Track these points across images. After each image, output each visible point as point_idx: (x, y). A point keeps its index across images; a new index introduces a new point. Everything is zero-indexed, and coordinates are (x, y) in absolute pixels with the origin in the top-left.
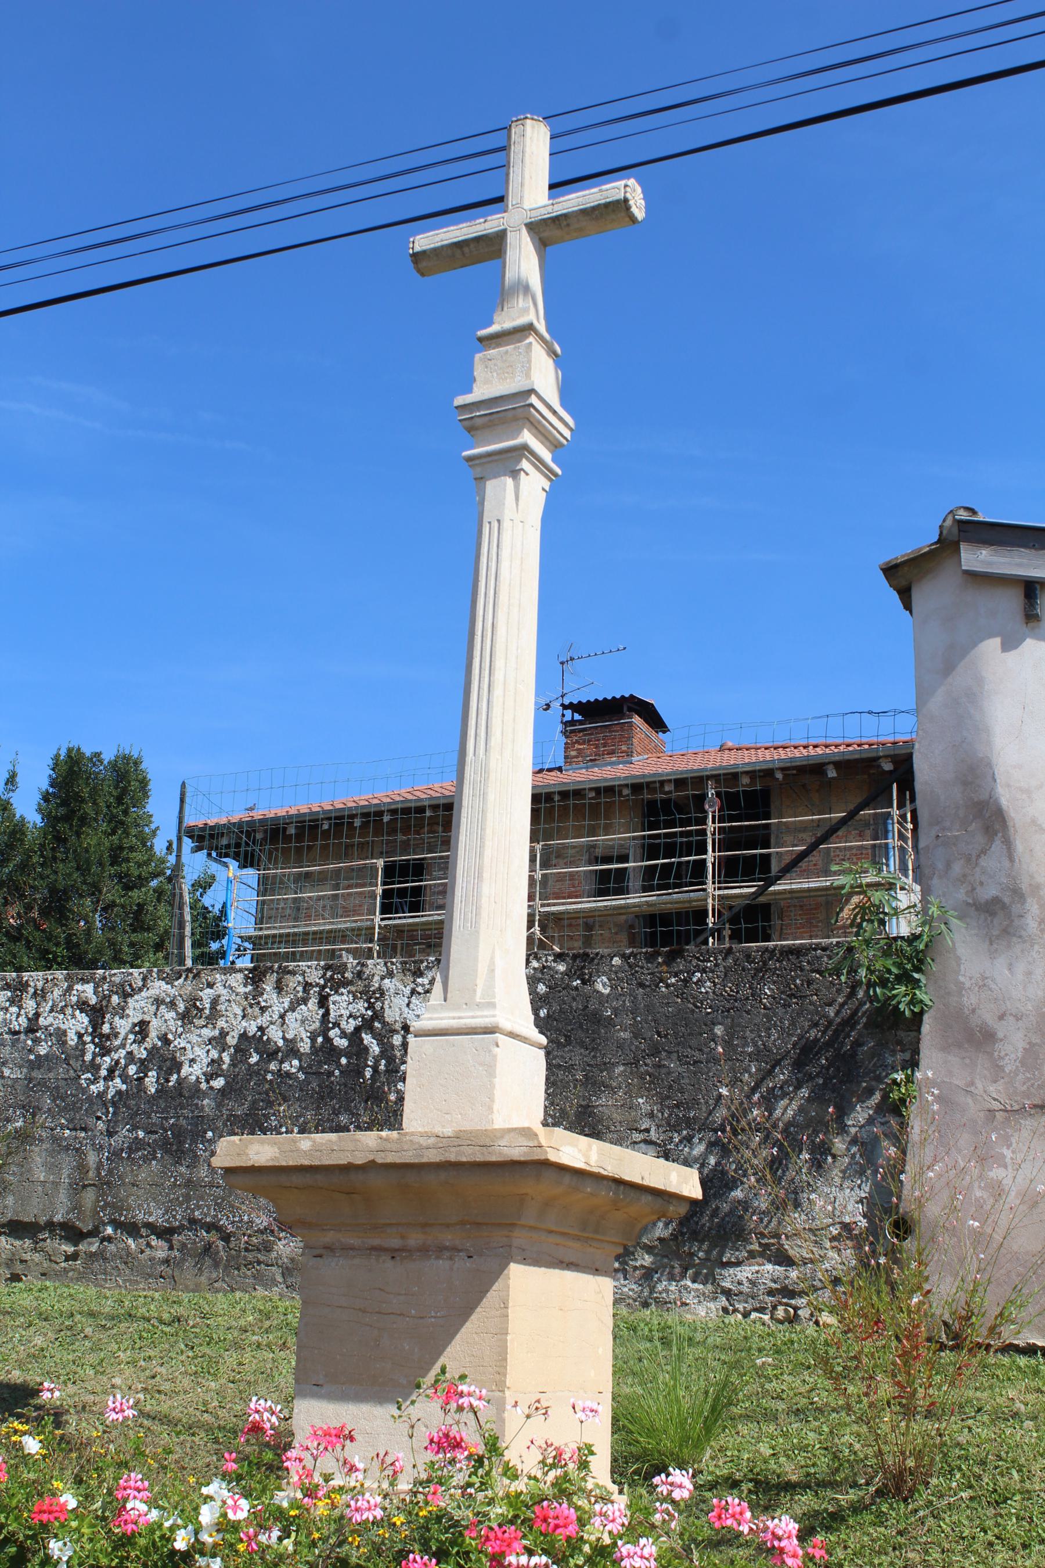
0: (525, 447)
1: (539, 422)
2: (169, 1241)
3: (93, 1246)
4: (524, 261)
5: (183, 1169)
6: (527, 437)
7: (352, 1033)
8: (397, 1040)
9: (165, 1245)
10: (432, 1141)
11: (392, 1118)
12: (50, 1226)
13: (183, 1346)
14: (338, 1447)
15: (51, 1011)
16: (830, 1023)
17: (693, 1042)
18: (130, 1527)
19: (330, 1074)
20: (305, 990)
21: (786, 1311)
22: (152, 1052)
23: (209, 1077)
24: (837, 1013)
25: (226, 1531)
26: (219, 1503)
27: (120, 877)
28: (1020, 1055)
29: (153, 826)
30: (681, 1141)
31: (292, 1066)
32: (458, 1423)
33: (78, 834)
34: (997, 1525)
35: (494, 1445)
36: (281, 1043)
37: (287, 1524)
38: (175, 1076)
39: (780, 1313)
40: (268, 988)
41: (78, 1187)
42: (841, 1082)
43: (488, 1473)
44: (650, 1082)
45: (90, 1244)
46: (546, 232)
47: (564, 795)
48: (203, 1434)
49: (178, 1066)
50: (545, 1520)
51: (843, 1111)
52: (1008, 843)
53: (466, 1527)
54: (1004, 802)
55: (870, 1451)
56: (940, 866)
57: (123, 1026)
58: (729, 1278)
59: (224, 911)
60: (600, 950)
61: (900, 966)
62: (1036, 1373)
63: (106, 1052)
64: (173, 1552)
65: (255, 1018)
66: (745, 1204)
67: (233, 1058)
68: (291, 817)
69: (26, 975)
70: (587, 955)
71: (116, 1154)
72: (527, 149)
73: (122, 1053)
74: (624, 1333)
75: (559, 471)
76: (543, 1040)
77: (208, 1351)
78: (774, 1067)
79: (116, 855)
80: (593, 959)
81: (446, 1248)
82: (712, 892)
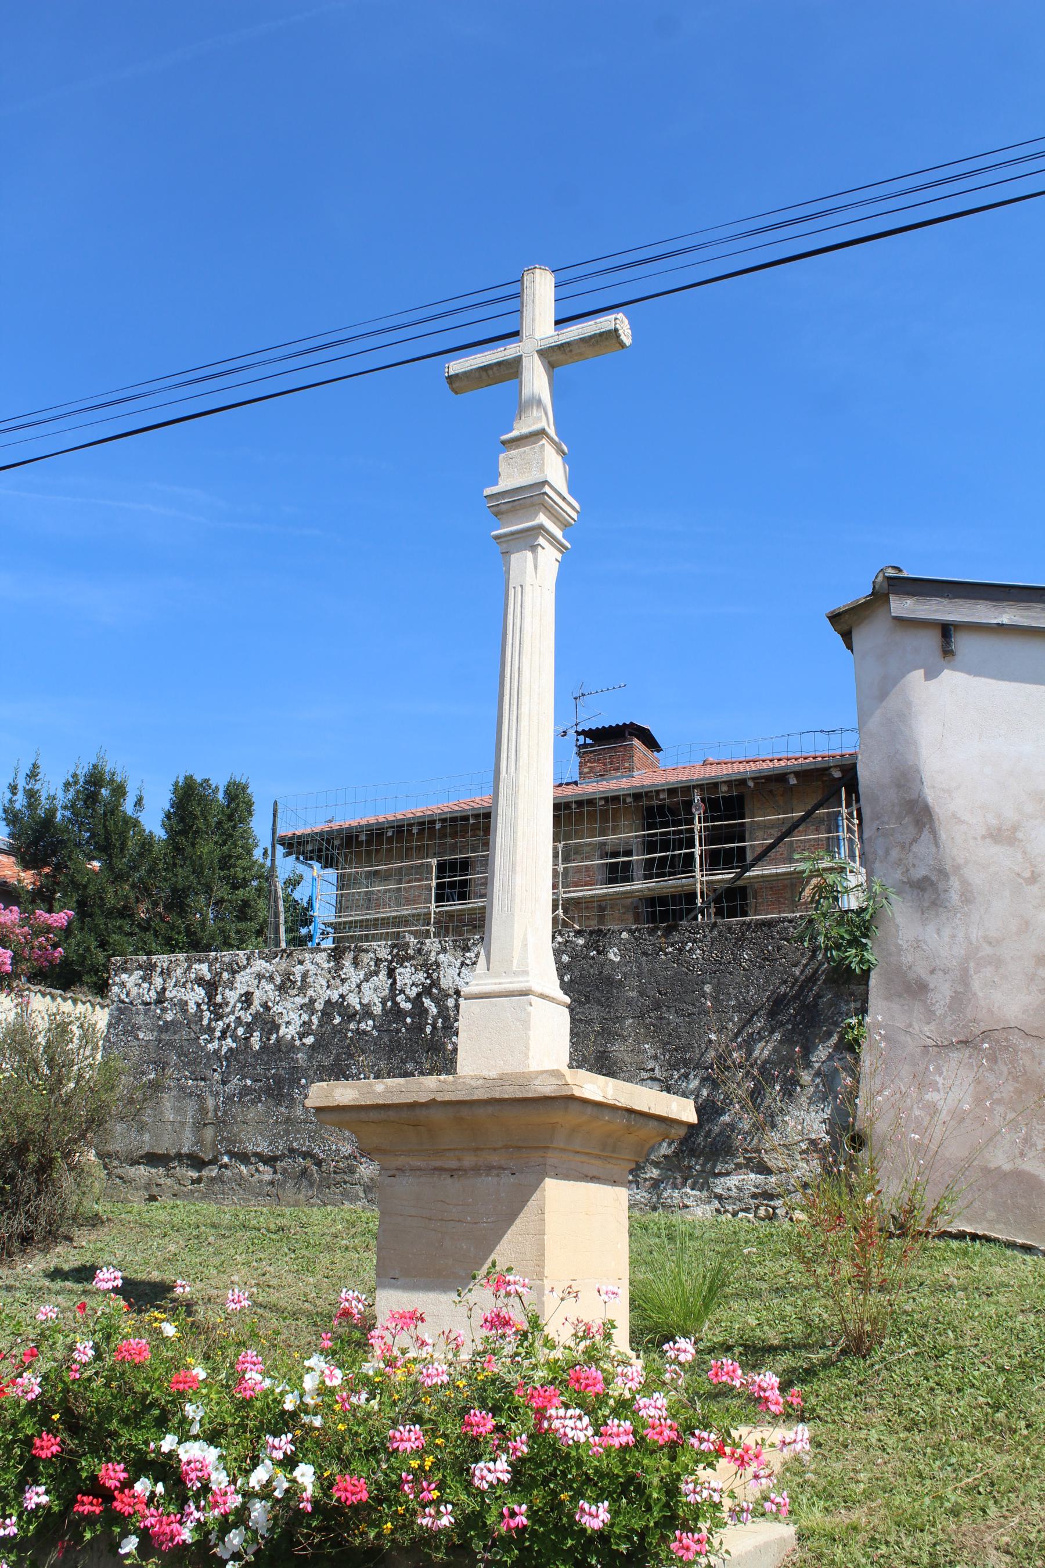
0: (541, 527)
1: (552, 507)
2: (274, 1167)
4: (536, 380)
5: (283, 1110)
6: (542, 519)
8: (451, 1003)
9: (271, 1170)
10: (481, 1082)
11: (447, 1063)
12: (179, 1156)
13: (286, 1250)
14: (412, 1327)
16: (796, 980)
17: (688, 998)
18: (249, 1393)
19: (398, 1031)
20: (376, 965)
21: (766, 1210)
22: (256, 1016)
23: (302, 1036)
25: (325, 1394)
26: (319, 1373)
27: (226, 878)
28: (947, 1001)
30: (679, 1078)
31: (368, 1025)
32: (506, 1305)
33: (193, 845)
34: (937, 1374)
35: (536, 1322)
36: (358, 1007)
38: (275, 1036)
39: (762, 1212)
41: (200, 1126)
42: (807, 1027)
43: (531, 1345)
46: (554, 356)
47: (580, 803)
48: (304, 1320)
49: (277, 1027)
50: (578, 1381)
51: (808, 1050)
52: (934, 832)
53: (515, 1388)
54: (930, 800)
55: (835, 1319)
56: (880, 852)
57: (232, 996)
58: (720, 1186)
61: (851, 933)
62: (965, 1253)
63: (219, 1017)
64: (284, 1412)
65: (337, 988)
66: (732, 1126)
67: (320, 1020)
68: (362, 826)
69: (154, 958)
70: (601, 931)
71: (229, 1098)
72: (537, 292)
73: (232, 1018)
74: (637, 1230)
75: (569, 546)
76: (568, 1000)
78: (752, 1017)
79: (225, 863)
80: (606, 934)
81: (494, 1167)
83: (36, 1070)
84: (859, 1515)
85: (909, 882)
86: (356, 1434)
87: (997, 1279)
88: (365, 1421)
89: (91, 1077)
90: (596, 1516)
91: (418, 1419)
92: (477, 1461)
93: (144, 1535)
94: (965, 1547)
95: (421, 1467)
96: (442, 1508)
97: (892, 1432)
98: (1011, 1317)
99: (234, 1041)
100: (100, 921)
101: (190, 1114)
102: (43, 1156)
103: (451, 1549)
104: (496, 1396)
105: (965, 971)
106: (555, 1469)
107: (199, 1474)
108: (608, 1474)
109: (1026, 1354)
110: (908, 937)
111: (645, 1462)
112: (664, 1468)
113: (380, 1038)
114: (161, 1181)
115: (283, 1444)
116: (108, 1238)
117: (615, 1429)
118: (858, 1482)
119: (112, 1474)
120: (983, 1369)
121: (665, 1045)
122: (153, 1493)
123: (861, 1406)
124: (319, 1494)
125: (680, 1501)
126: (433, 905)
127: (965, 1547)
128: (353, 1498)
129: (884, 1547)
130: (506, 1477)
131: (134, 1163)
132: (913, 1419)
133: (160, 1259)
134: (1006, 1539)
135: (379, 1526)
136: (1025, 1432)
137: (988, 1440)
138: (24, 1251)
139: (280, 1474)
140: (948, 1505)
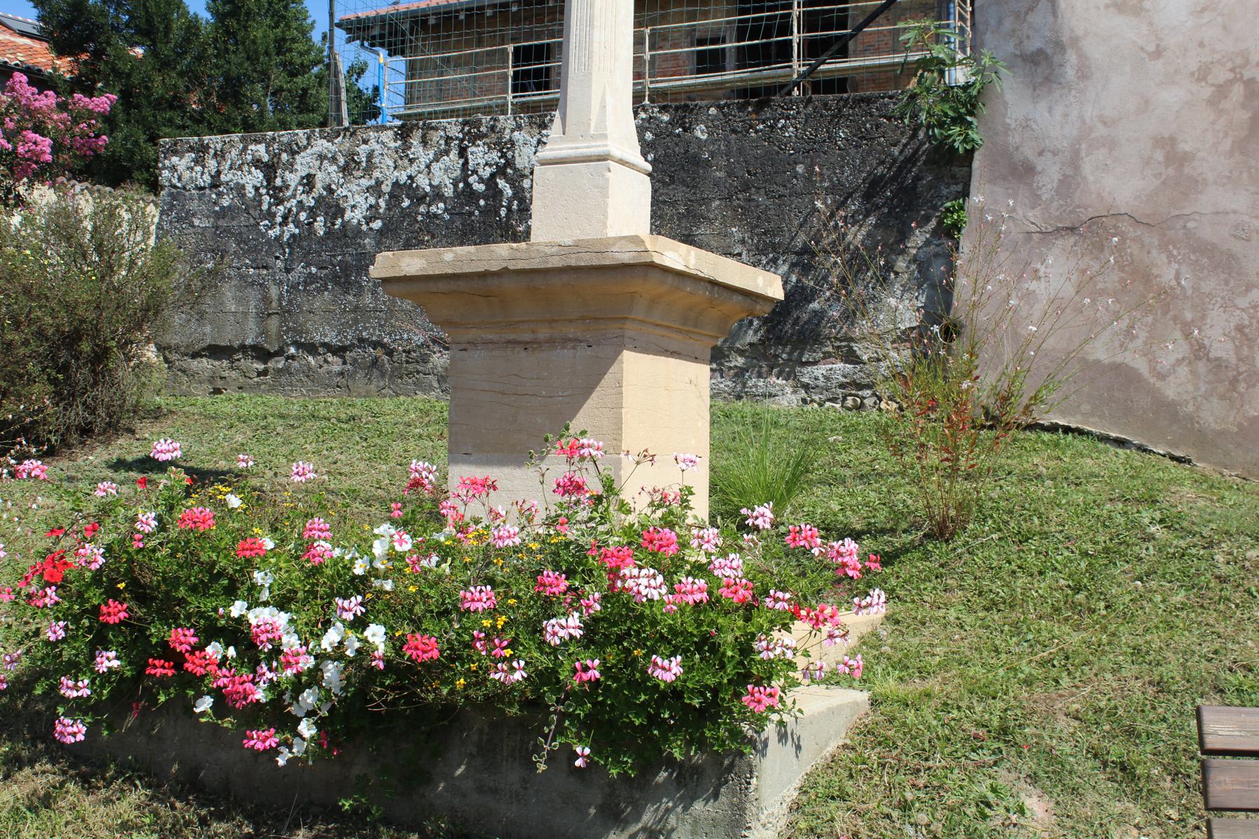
2: (343, 357)
3: (280, 363)
5: (351, 298)
7: (489, 179)
9: (340, 361)
10: (555, 249)
12: (243, 348)
14: (484, 495)
15: (231, 168)
16: (895, 160)
17: (779, 180)
18: (317, 559)
20: (447, 144)
21: (854, 400)
22: (319, 200)
23: (369, 220)
24: (901, 152)
25: (395, 559)
26: (388, 539)
27: (283, 64)
28: (1055, 185)
29: (309, 21)
32: (580, 469)
33: (246, 28)
34: (1020, 558)
35: (610, 486)
36: (428, 189)
37: (445, 553)
38: (340, 220)
40: (415, 143)
41: (264, 316)
42: (903, 211)
44: (742, 214)
45: (277, 362)
49: (341, 212)
51: (904, 234)
55: (920, 504)
56: (993, 22)
57: (293, 179)
58: (807, 374)
59: (376, 89)
60: (699, 102)
61: (955, 110)
62: (1057, 445)
63: (280, 202)
64: (355, 577)
69: (206, 139)
70: (687, 106)
71: (294, 287)
73: (294, 202)
77: (379, 441)
78: (846, 199)
79: (281, 45)
81: (570, 340)
82: (798, 67)
83: (84, 256)
84: (933, 684)
85: (1021, 56)
86: (428, 596)
87: (1087, 470)
88: (437, 584)
89: (145, 264)
90: (668, 670)
91: (490, 581)
92: (549, 619)
93: (218, 694)
94: (1035, 712)
95: (494, 627)
96: (515, 664)
97: (971, 611)
98: (1098, 506)
99: (296, 227)
100: (147, 112)
101: (252, 304)
102: (97, 346)
103: (527, 704)
104: (574, 563)
105: (1076, 153)
106: (630, 628)
107: (270, 636)
108: (682, 633)
109: (1111, 540)
110: (1016, 111)
111: (720, 621)
112: (739, 628)
113: (452, 221)
114: (225, 374)
115: (353, 606)
116: (172, 430)
117: (689, 587)
118: (934, 655)
119: (182, 639)
120: (1066, 553)
121: (753, 228)
122: (225, 658)
123: (941, 588)
124: (391, 654)
125: (753, 660)
126: (510, 97)
127: (1035, 712)
128: (425, 656)
129: (955, 712)
130: (578, 633)
131: (195, 355)
132: (992, 600)
133: (227, 449)
134: (1076, 706)
135: (452, 683)
136: (1104, 612)
137: (1066, 619)
138: (83, 443)
139: (351, 634)
140: (1021, 676)
